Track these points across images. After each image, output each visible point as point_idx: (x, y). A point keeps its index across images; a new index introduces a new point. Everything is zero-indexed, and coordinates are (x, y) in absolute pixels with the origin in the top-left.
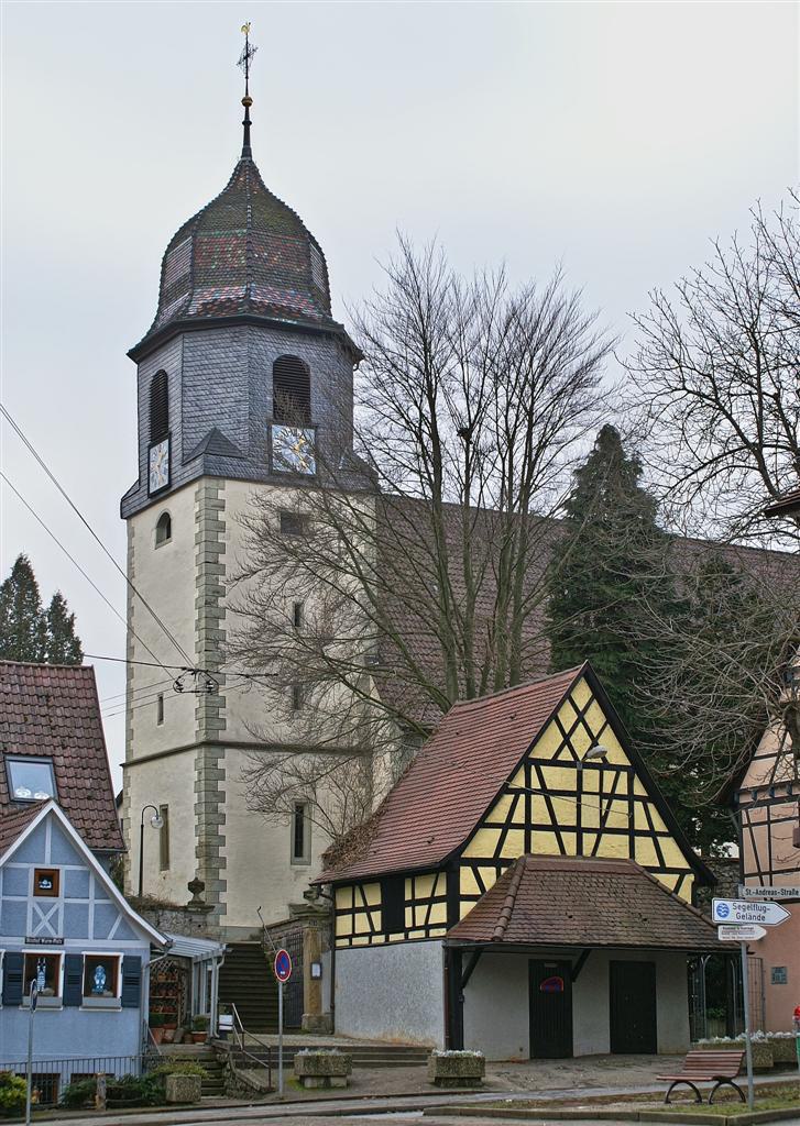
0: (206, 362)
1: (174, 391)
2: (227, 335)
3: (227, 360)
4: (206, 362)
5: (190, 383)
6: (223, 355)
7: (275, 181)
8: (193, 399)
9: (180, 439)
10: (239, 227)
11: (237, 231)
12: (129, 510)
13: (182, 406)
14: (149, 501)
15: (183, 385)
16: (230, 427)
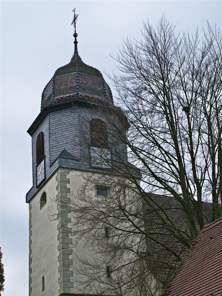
0: (60, 123)
1: (46, 138)
2: (69, 111)
3: (69, 121)
4: (60, 123)
5: (53, 133)
6: (67, 119)
7: (87, 60)
8: (54, 139)
9: (49, 157)
10: (73, 72)
11: (72, 73)
12: (29, 199)
13: (50, 142)
14: (37, 190)
15: (50, 134)
16: (71, 148)
